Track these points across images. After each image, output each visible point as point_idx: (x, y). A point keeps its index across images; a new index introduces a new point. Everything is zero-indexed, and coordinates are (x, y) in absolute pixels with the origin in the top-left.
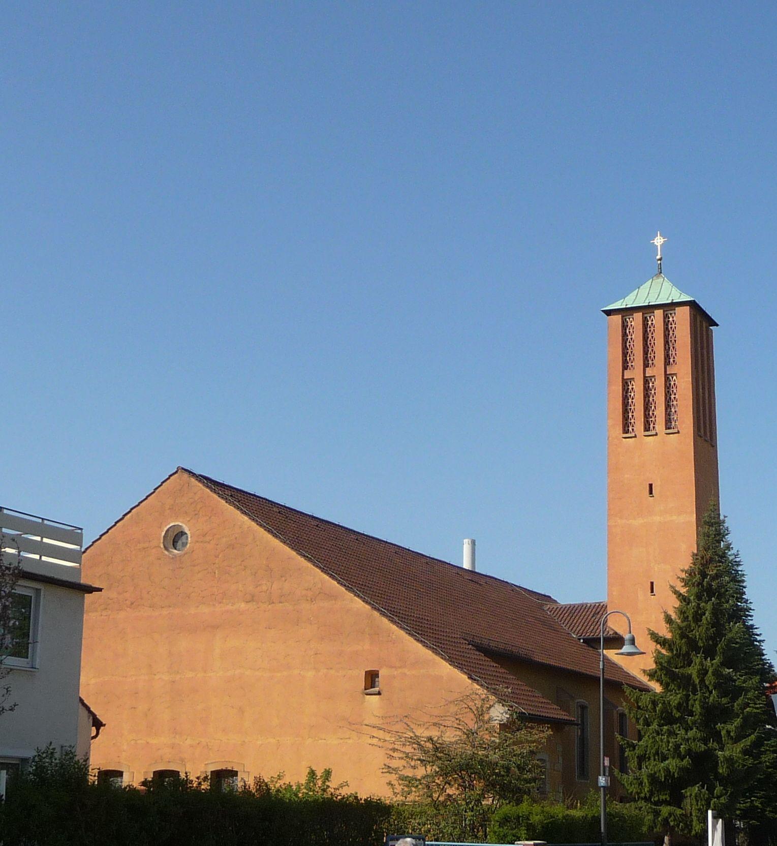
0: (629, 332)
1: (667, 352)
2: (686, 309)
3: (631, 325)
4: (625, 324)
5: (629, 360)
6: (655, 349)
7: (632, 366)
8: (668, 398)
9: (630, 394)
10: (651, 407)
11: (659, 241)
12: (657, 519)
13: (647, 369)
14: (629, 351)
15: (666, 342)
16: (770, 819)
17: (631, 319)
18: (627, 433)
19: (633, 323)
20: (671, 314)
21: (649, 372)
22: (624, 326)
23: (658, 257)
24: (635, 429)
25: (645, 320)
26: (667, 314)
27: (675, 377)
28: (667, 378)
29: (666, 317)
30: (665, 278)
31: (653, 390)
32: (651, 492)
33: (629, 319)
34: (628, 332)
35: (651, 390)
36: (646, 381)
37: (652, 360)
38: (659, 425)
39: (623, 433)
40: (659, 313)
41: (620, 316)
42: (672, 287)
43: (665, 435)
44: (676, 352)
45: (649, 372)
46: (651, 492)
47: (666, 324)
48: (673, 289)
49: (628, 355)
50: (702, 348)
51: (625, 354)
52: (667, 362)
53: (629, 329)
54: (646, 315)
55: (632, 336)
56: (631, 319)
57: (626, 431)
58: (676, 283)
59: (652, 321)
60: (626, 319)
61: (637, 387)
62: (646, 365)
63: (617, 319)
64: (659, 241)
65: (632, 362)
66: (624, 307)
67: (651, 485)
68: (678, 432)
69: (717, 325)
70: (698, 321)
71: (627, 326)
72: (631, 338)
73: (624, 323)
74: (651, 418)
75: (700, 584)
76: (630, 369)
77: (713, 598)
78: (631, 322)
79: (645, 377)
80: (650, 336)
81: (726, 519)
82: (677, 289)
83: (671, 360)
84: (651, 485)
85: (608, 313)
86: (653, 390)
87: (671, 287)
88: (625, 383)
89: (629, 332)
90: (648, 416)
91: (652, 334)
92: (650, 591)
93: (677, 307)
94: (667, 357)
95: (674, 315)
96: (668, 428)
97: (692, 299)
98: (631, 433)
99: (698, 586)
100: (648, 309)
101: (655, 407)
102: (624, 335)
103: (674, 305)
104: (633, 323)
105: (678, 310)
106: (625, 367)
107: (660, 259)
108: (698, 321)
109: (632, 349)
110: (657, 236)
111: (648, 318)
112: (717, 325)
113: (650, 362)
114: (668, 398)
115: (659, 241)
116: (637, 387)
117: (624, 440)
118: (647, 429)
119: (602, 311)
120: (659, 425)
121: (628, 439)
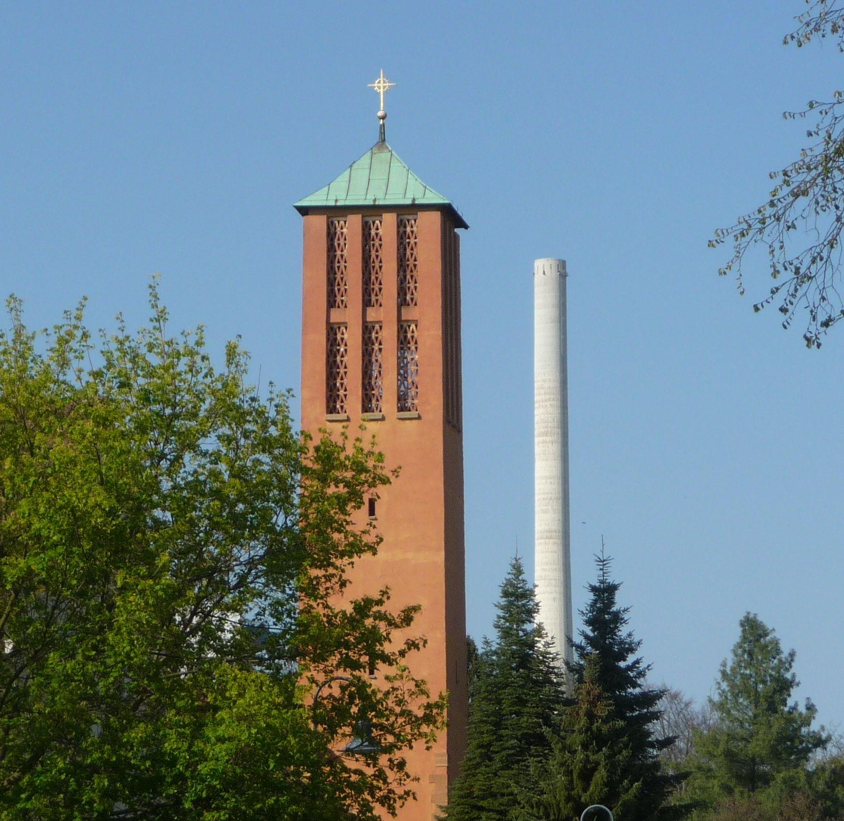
0: (339, 245)
2: (436, 216)
3: (342, 233)
4: (333, 230)
6: (380, 276)
7: (342, 301)
11: (381, 85)
13: (369, 310)
16: (46, 654)
17: (342, 223)
18: (331, 413)
19: (345, 230)
21: (372, 315)
22: (331, 235)
23: (380, 113)
24: (345, 406)
25: (366, 227)
28: (402, 327)
29: (401, 224)
30: (393, 152)
31: (377, 345)
34: (336, 244)
36: (367, 329)
37: (376, 295)
38: (388, 404)
39: (327, 413)
40: (390, 219)
41: (325, 216)
42: (408, 170)
44: (417, 285)
47: (402, 237)
48: (410, 175)
49: (336, 284)
51: (331, 282)
52: (403, 302)
53: (339, 240)
54: (367, 219)
55: (342, 251)
56: (342, 223)
57: (331, 409)
58: (413, 167)
59: (377, 229)
61: (352, 338)
62: (367, 303)
63: (320, 221)
64: (381, 85)
65: (342, 296)
66: (332, 203)
68: (419, 418)
69: (466, 227)
70: (448, 227)
71: (335, 233)
72: (342, 256)
75: (588, 729)
76: (339, 307)
77: (604, 749)
78: (342, 228)
79: (364, 322)
81: (157, 286)
82: (416, 177)
83: (408, 297)
85: (304, 211)
86: (377, 345)
87: (405, 172)
88: (332, 330)
89: (339, 245)
91: (377, 251)
93: (420, 211)
94: (402, 291)
95: (413, 222)
96: (401, 409)
97: (446, 202)
98: (338, 413)
99: (586, 732)
100: (375, 210)
101: (380, 372)
102: (331, 249)
103: (415, 208)
104: (345, 230)
105: (423, 216)
106: (331, 303)
107: (383, 118)
108: (448, 227)
109: (342, 273)
110: (380, 77)
112: (466, 227)
113: (373, 298)
115: (381, 85)
116: (352, 338)
117: (328, 423)
118: (366, 409)
119: (295, 207)
120: (388, 404)
121: (334, 424)
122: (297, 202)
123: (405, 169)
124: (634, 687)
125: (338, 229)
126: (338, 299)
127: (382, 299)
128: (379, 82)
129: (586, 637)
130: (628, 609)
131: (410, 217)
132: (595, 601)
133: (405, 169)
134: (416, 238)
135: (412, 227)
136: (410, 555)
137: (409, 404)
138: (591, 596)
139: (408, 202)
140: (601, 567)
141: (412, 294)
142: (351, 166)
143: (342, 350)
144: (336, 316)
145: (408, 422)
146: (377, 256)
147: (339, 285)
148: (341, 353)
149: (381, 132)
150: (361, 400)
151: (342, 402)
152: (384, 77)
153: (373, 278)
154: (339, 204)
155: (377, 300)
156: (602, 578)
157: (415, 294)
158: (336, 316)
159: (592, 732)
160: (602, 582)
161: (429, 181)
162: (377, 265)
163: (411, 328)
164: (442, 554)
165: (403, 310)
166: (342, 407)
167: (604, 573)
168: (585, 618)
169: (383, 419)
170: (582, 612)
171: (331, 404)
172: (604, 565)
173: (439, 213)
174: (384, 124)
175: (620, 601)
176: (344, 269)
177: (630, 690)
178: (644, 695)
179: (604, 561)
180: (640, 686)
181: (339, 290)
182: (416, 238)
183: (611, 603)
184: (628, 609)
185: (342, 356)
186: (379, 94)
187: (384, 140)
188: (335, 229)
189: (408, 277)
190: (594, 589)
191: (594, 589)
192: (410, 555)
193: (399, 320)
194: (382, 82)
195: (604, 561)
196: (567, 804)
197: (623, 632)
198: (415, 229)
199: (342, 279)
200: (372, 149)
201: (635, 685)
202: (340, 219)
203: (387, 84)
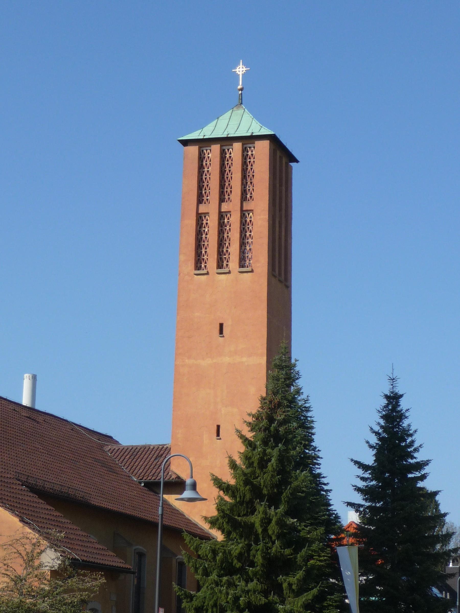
0: (206, 164)
1: (245, 187)
3: (209, 157)
4: (203, 155)
5: (204, 194)
8: (243, 235)
9: (204, 229)
10: (225, 244)
11: (241, 70)
12: (227, 360)
13: (223, 204)
14: (205, 184)
15: (244, 177)
20: (250, 148)
22: (201, 158)
23: (239, 87)
24: (207, 266)
26: (246, 148)
27: (251, 214)
28: (243, 214)
29: (244, 150)
32: (221, 332)
33: (207, 150)
34: (204, 164)
35: (226, 226)
36: (221, 216)
40: (237, 146)
43: (239, 273)
45: (225, 207)
46: (221, 332)
47: (245, 157)
50: (281, 185)
51: (200, 187)
52: (244, 198)
53: (206, 161)
54: (224, 148)
55: (208, 168)
58: (257, 116)
59: (230, 154)
60: (203, 151)
62: (222, 200)
63: (194, 150)
64: (241, 70)
65: (207, 197)
67: (221, 325)
68: (252, 271)
69: (297, 161)
72: (208, 171)
73: (201, 155)
74: (225, 255)
76: (205, 203)
78: (208, 154)
80: (227, 169)
82: (257, 122)
84: (221, 325)
85: (185, 143)
86: (228, 226)
88: (200, 217)
89: (206, 164)
90: (222, 253)
92: (216, 434)
97: (273, 133)
101: (229, 244)
102: (201, 167)
103: (253, 138)
104: (210, 155)
106: (200, 200)
107: (241, 89)
109: (208, 182)
111: (227, 150)
112: (297, 161)
113: (227, 197)
114: (243, 235)
115: (241, 70)
117: (196, 276)
118: (220, 266)
121: (199, 276)
122: (180, 138)
123: (251, 118)
124: (412, 459)
125: (206, 155)
126: (205, 198)
127: (231, 197)
128: (239, 68)
129: (382, 427)
130: (408, 409)
131: (251, 145)
132: (388, 404)
133: (251, 118)
134: (254, 159)
135: (252, 152)
136: (244, 359)
137: (247, 263)
138: (385, 402)
139: (249, 134)
140: (392, 383)
141: (251, 194)
142: (218, 118)
143: (206, 230)
144: (203, 209)
145: (245, 274)
146: (230, 171)
147: (205, 189)
148: (205, 232)
149: (240, 99)
150: (216, 261)
151: (206, 263)
152: (242, 65)
153: (227, 184)
154: (205, 137)
155: (229, 198)
156: (392, 390)
157: (253, 193)
158: (203, 209)
159: (270, 431)
160: (392, 393)
161: (263, 123)
162: (229, 176)
163: (250, 215)
164: (265, 358)
165: (244, 203)
166: (205, 266)
167: (393, 387)
168: (380, 415)
169: (229, 272)
170: (379, 411)
171: (199, 265)
172: (393, 382)
173: (269, 141)
174: (242, 94)
175: (404, 404)
176: (209, 179)
177: (410, 460)
178: (418, 463)
179: (394, 379)
180: (415, 458)
181: (205, 193)
182: (254, 159)
183: (397, 405)
184: (408, 409)
185: (207, 234)
186: (239, 75)
187: (242, 103)
188: (205, 155)
189: (249, 183)
190: (387, 397)
191: (387, 397)
192: (244, 359)
193: (242, 210)
194: (241, 68)
195: (394, 379)
196: (246, 486)
197: (405, 423)
198: (254, 153)
199: (207, 185)
200: (233, 108)
201: (413, 457)
202: (207, 148)
203: (245, 69)
